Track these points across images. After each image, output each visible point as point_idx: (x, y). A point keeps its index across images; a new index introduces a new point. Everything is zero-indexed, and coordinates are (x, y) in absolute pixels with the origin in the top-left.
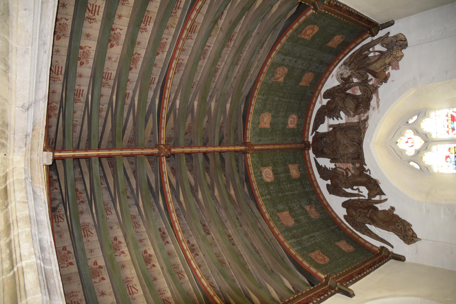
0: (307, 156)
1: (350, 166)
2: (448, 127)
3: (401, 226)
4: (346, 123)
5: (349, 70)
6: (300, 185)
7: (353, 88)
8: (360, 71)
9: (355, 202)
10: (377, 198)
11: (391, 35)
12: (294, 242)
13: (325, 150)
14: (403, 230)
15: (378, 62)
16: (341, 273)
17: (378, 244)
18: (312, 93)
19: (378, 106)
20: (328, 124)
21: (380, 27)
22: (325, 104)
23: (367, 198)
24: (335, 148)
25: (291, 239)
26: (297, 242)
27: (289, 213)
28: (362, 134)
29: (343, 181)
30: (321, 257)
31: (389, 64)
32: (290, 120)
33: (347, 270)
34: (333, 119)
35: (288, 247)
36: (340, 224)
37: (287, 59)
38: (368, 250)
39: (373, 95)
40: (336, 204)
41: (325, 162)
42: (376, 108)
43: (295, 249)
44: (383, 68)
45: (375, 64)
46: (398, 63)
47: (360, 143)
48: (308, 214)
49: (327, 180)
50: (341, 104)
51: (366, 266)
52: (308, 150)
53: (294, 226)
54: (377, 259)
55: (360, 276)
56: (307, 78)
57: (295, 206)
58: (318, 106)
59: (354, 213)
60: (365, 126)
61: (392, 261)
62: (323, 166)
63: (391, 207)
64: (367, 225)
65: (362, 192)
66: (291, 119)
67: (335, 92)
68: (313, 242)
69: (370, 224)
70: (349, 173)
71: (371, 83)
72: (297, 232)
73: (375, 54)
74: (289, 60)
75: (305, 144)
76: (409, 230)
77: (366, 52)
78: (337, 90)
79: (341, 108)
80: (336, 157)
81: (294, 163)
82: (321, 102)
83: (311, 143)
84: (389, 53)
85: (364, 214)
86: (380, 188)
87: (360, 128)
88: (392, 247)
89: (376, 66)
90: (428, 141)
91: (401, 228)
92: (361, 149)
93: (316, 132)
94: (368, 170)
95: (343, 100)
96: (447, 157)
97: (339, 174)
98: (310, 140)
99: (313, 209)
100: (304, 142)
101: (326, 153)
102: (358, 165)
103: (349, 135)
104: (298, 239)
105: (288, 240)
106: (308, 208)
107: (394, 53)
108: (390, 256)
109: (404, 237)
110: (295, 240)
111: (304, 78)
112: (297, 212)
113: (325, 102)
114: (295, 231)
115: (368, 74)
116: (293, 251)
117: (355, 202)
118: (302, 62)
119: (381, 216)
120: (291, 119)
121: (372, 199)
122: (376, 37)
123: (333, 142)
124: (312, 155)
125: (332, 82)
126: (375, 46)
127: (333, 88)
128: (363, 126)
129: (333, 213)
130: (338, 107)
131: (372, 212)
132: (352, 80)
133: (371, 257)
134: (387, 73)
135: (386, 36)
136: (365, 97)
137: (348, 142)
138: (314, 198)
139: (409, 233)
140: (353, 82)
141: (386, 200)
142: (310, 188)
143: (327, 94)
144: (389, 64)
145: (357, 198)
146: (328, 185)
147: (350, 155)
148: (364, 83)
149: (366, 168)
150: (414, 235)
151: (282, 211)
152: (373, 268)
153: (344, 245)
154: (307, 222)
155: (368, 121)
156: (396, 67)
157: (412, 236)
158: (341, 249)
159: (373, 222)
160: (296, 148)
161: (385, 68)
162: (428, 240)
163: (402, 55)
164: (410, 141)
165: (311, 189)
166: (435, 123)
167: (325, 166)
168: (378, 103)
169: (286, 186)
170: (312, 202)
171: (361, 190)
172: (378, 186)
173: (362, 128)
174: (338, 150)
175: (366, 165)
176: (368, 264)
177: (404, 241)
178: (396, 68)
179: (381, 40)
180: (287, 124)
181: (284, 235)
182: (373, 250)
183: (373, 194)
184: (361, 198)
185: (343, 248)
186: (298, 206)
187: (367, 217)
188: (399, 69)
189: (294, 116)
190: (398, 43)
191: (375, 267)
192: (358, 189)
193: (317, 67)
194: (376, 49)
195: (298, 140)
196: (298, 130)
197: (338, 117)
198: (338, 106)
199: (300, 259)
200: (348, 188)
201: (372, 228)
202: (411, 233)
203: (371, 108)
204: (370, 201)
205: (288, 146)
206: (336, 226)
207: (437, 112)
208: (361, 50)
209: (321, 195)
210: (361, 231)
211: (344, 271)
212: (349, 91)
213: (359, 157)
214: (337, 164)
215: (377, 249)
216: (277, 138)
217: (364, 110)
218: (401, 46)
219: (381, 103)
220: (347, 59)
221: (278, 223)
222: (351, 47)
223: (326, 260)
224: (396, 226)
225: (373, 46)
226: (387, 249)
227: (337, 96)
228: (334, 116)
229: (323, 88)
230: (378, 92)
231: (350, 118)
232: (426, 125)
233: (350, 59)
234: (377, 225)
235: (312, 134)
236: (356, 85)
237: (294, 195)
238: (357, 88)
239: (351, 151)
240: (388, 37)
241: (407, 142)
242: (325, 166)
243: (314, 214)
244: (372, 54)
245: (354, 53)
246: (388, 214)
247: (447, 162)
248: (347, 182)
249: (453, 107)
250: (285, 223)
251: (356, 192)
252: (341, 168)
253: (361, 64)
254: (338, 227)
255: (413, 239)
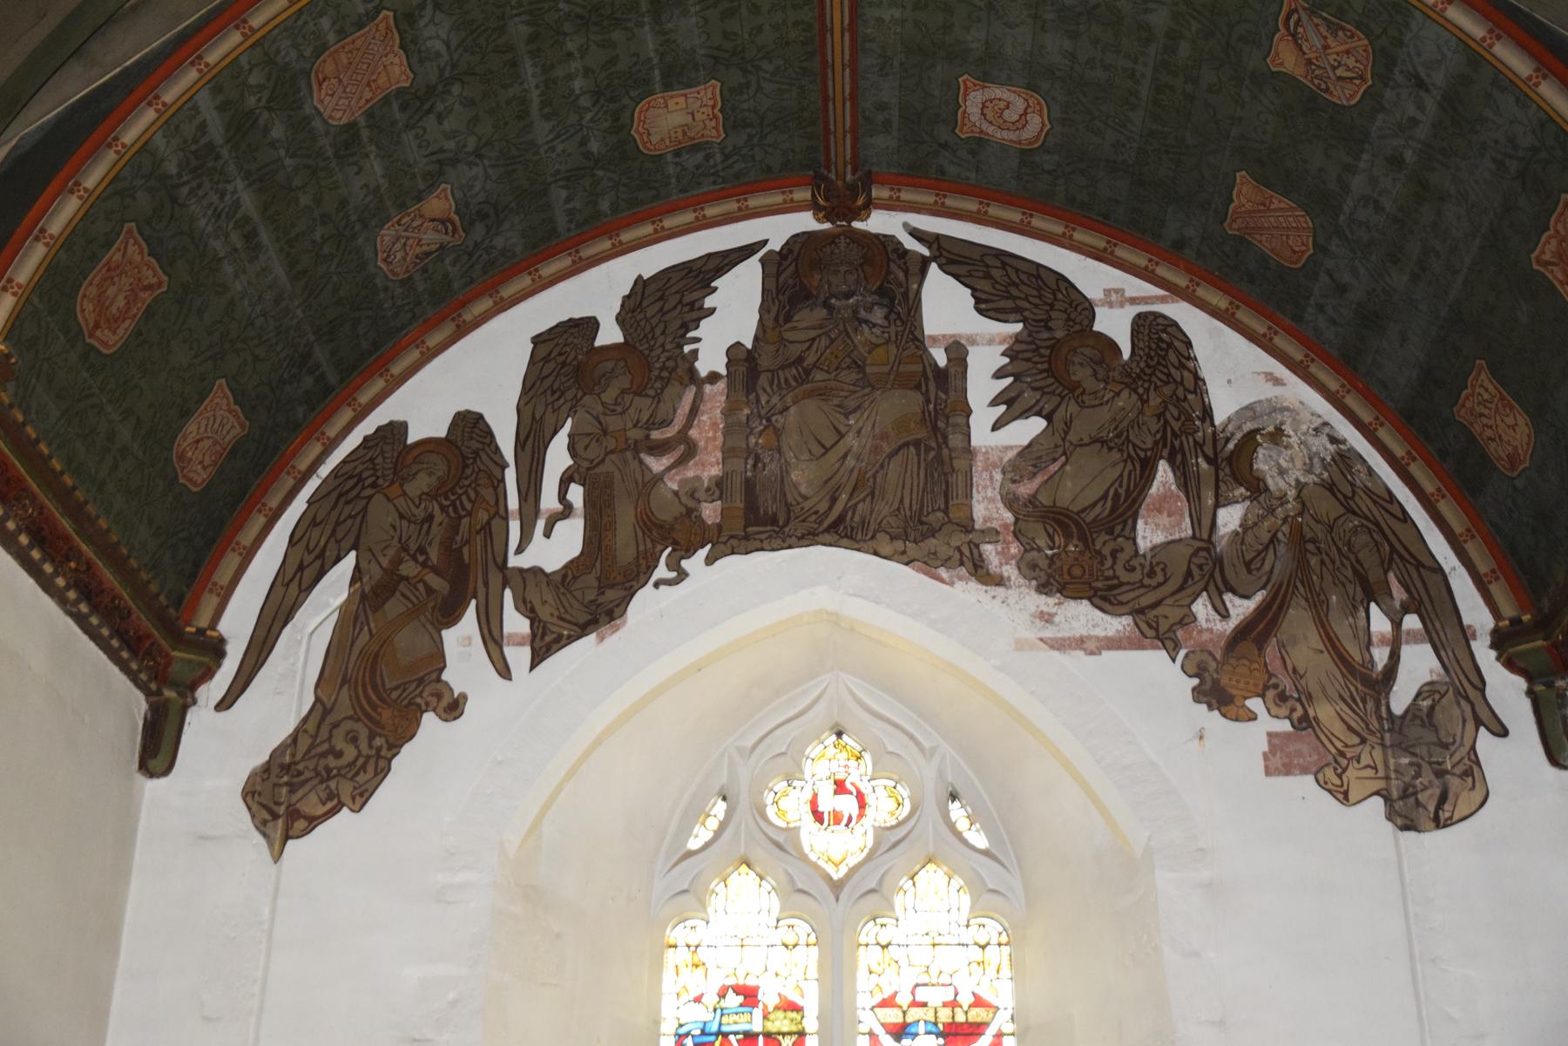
0: (776, 198)
1: (708, 467)
2: (915, 1004)
3: (350, 753)
4: (969, 452)
5: (1300, 486)
6: (588, 155)
7: (1183, 504)
8: (1282, 549)
9: (487, 493)
10: (515, 623)
11: (1485, 743)
12: (203, 127)
13: (808, 318)
14: (332, 762)
15: (1326, 661)
16: (29, 429)
17: (237, 622)
18: (1179, 245)
19: (1060, 645)
20: (973, 341)
21: (1550, 685)
22: (1098, 327)
23: (514, 561)
24: (819, 376)
25: (221, 108)
26: (210, 147)
27: (400, 92)
28: (899, 545)
29: (614, 423)
30: (121, 302)
31: (1306, 716)
32: (1014, 100)
33: (57, 465)
34: (999, 375)
35: (168, 97)
36: (349, 399)
37: (1421, 107)
38: (197, 565)
39: (1127, 621)
40: (472, 377)
41: (733, 315)
42: (1049, 633)
43: (159, 141)
44: (1286, 683)
45: (1315, 639)
46: (1304, 771)
47: (842, 530)
48: (402, 206)
49: (621, 320)
50: (1088, 423)
51: (89, 565)
52: (814, 206)
53: (317, 123)
54: (143, 621)
55: (24, 539)
56: (1279, 226)
57: (447, 126)
58: (1089, 276)
59: (422, 483)
60: (946, 563)
61: (139, 704)
62: (709, 302)
63: (464, 697)
64: (350, 560)
65: (547, 534)
66: (1020, 104)
67: (1167, 390)
68: (216, 244)
69: (353, 581)
70: (666, 461)
71: (1202, 608)
72: (273, 144)
73: (1383, 642)
74: (1414, 122)
75: (853, 190)
76: (330, 797)
77: (1399, 594)
78: (1179, 401)
79: (1068, 425)
80: (763, 380)
81: (732, 118)
82: (1114, 296)
83: (857, 225)
84: (1375, 724)
85: (413, 547)
86: (571, 639)
87: (933, 533)
88: (224, 704)
89: (1300, 642)
90: (839, 904)
91: (339, 755)
92: (809, 538)
93: (924, 264)
94: (682, 575)
95: (1115, 441)
96: (749, 996)
97: (658, 398)
98: (880, 223)
99: (431, 237)
100: (868, 180)
101: (788, 319)
102: (710, 512)
103: (894, 467)
104: (225, 152)
105: (217, 90)
106: (439, 203)
107: (1372, 754)
108: (169, 694)
109: (286, 768)
110: (216, 132)
111: (1279, 202)
112: (408, 138)
113: (1115, 324)
114: (277, 132)
115: (1259, 597)
116: (138, 127)
117: (487, 493)
118: (1387, 204)
119: (407, 641)
120: (1020, 104)
121: (508, 594)
122: (1485, 656)
123: (859, 366)
124: (778, 230)
125: (1236, 373)
126: (1428, 647)
127: (1198, 379)
128: (944, 551)
129: (415, 355)
130: (1073, 408)
131: (430, 591)
132: (1230, 502)
133: (154, 588)
134: (1255, 704)
135: (1484, 714)
136: (1120, 571)
137: (850, 462)
138: (510, 237)
139: (313, 798)
140: (1217, 505)
141: (504, 672)
142: (571, 212)
143: (1158, 337)
144: (1304, 723)
145: (513, 502)
146: (589, 325)
147: (772, 468)
148: (1209, 569)
149: (694, 563)
150: (300, 824)
151: (410, 45)
152: (84, 608)
153: (209, 432)
154: (343, 203)
155: (973, 585)
156: (1280, 760)
157: (294, 814)
158: (185, 415)
159: (368, 598)
160: (827, 131)
161: (1283, 698)
162: (275, 898)
163: (1353, 797)
164: (848, 804)
165: (561, 221)
166: (937, 946)
167: (712, 311)
168: (1079, 643)
169: (575, 65)
170: (479, 230)
171: (560, 526)
172: (583, 630)
173: (932, 543)
174: (809, 395)
175: (710, 561)
176: (108, 576)
177: (266, 769)
178: (1277, 761)
179: (1462, 684)
180: (986, 78)
181: (244, 61)
182: (197, 598)
183: (533, 596)
184: (515, 527)
185: (192, 429)
186: (450, 145)
187: (397, 562)
188: (1268, 772)
189: (1035, 123)
190: (1427, 777)
191: (94, 621)
192: (567, 511)
193: (1342, 289)
194: (1407, 651)
195: (882, 144)
196: (945, 146)
197: (1012, 405)
198: (1082, 405)
199: (94, 177)
200: (572, 449)
201: (334, 589)
202: (312, 806)
203: (1047, 603)
204: (495, 578)
205: (841, 82)
206: (332, 378)
207: (998, 956)
208: (1419, 565)
209: (525, 281)
210: (314, 523)
211: (44, 448)
212: (1164, 474)
213: (762, 518)
214: (721, 385)
215: (203, 621)
216: (897, 13)
217: (1044, 563)
218: (1404, 795)
219: (1077, 660)
220: (1370, 471)
221: (325, 23)
222: (1446, 507)
223: (105, 334)
224: (349, 725)
225: (1432, 636)
226: (208, 674)
227: (1144, 402)
228: (1017, 377)
229: (1202, 316)
230: (1142, 647)
231: (998, 477)
232: (933, 901)
233: (1368, 492)
234: (349, 620)
235: (916, 234)
236: (1196, 522)
237: (523, 115)
238: (1179, 524)
239: (795, 476)
240: (1479, 723)
241: (840, 788)
242: (712, 311)
243: (404, 242)
244: (1380, 623)
245: (1405, 517)
246: (421, 681)
247: (722, 995)
248: (610, 443)
249: (1019, 1035)
250: (329, 68)
251: (549, 500)
252: (694, 411)
253: (1333, 555)
254: (328, 390)
255: (275, 817)
